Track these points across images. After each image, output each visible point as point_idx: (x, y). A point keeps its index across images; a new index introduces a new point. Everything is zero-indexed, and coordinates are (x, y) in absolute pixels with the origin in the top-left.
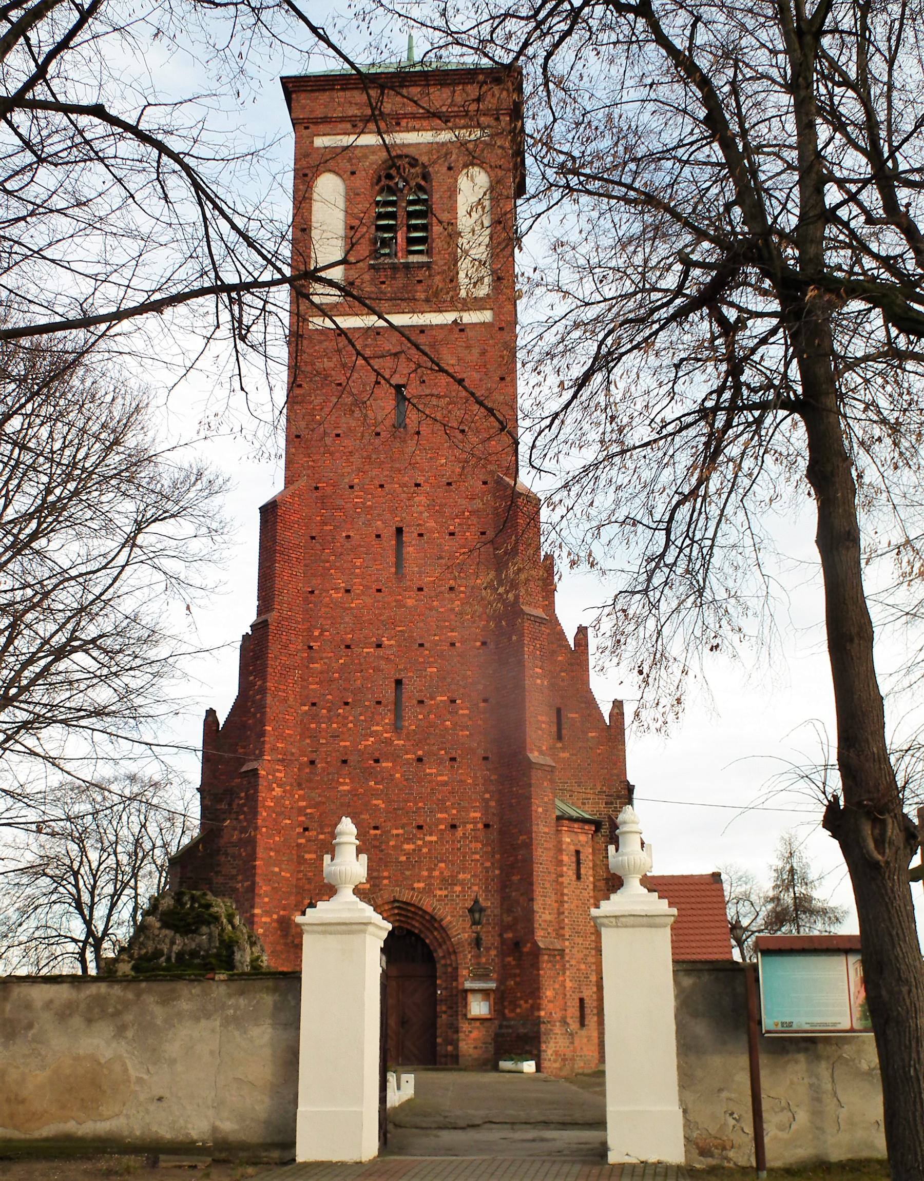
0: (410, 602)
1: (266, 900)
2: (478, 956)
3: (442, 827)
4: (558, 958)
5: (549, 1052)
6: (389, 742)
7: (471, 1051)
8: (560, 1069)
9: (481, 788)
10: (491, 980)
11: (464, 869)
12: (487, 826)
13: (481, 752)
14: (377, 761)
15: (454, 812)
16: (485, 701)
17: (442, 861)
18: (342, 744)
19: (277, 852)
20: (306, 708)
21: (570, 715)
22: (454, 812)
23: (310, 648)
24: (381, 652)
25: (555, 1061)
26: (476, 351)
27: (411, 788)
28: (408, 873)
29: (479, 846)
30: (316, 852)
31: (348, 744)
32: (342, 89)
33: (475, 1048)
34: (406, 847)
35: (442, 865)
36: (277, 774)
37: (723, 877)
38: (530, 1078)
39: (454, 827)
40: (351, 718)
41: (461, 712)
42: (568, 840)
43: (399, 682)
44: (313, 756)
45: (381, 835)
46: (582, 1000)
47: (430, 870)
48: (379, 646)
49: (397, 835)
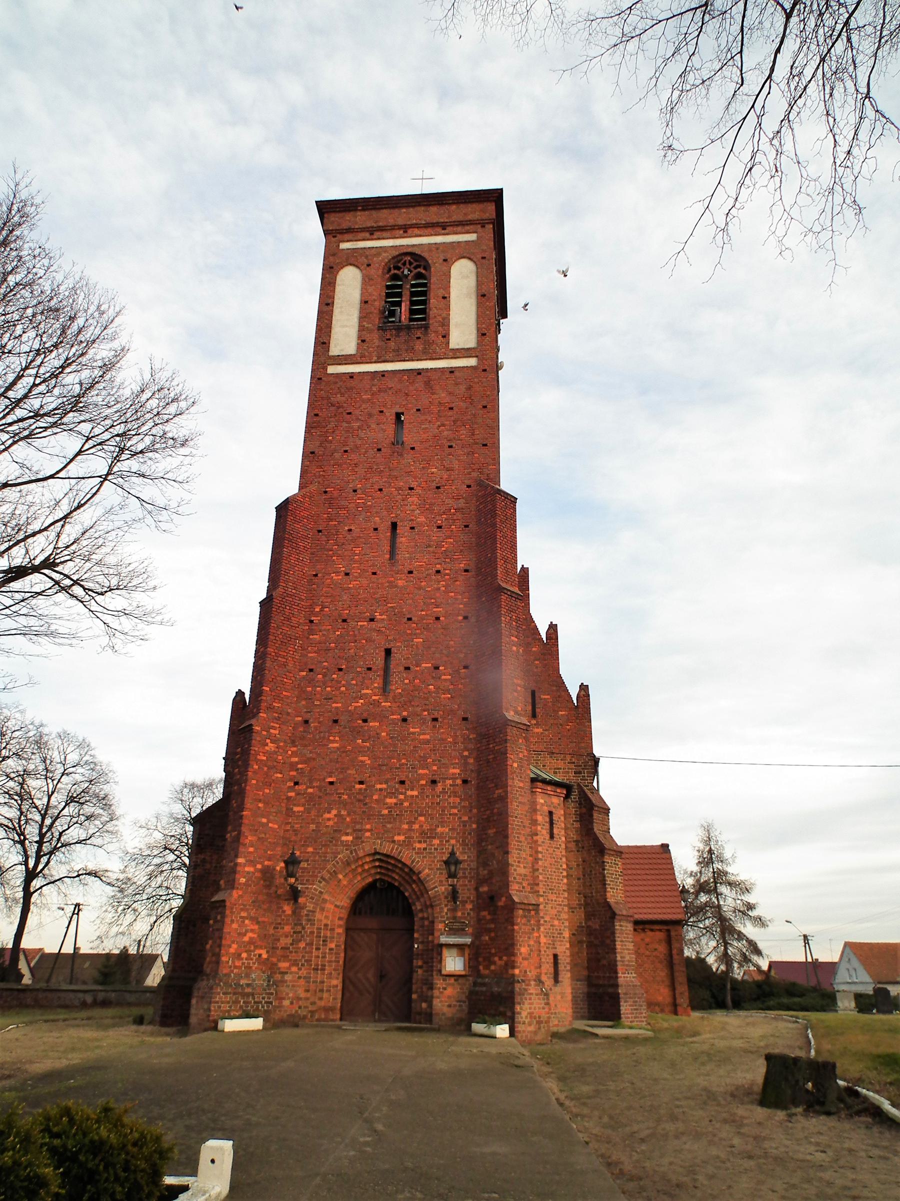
1: (251, 849)
2: (454, 910)
3: (423, 782)
5: (524, 1014)
6: (377, 704)
7: (445, 1009)
8: (535, 1033)
10: (467, 934)
11: (442, 823)
12: (465, 782)
14: (365, 721)
15: (435, 768)
18: (334, 705)
19: (266, 803)
20: (304, 673)
22: (435, 768)
24: (373, 625)
26: (463, 388)
27: (395, 745)
28: (389, 826)
30: (303, 805)
32: (363, 210)
33: (450, 1006)
34: (388, 800)
35: (422, 819)
36: (272, 731)
39: (434, 782)
42: (542, 801)
44: (307, 716)
45: (366, 790)
46: (555, 956)
47: (411, 823)
48: (372, 620)
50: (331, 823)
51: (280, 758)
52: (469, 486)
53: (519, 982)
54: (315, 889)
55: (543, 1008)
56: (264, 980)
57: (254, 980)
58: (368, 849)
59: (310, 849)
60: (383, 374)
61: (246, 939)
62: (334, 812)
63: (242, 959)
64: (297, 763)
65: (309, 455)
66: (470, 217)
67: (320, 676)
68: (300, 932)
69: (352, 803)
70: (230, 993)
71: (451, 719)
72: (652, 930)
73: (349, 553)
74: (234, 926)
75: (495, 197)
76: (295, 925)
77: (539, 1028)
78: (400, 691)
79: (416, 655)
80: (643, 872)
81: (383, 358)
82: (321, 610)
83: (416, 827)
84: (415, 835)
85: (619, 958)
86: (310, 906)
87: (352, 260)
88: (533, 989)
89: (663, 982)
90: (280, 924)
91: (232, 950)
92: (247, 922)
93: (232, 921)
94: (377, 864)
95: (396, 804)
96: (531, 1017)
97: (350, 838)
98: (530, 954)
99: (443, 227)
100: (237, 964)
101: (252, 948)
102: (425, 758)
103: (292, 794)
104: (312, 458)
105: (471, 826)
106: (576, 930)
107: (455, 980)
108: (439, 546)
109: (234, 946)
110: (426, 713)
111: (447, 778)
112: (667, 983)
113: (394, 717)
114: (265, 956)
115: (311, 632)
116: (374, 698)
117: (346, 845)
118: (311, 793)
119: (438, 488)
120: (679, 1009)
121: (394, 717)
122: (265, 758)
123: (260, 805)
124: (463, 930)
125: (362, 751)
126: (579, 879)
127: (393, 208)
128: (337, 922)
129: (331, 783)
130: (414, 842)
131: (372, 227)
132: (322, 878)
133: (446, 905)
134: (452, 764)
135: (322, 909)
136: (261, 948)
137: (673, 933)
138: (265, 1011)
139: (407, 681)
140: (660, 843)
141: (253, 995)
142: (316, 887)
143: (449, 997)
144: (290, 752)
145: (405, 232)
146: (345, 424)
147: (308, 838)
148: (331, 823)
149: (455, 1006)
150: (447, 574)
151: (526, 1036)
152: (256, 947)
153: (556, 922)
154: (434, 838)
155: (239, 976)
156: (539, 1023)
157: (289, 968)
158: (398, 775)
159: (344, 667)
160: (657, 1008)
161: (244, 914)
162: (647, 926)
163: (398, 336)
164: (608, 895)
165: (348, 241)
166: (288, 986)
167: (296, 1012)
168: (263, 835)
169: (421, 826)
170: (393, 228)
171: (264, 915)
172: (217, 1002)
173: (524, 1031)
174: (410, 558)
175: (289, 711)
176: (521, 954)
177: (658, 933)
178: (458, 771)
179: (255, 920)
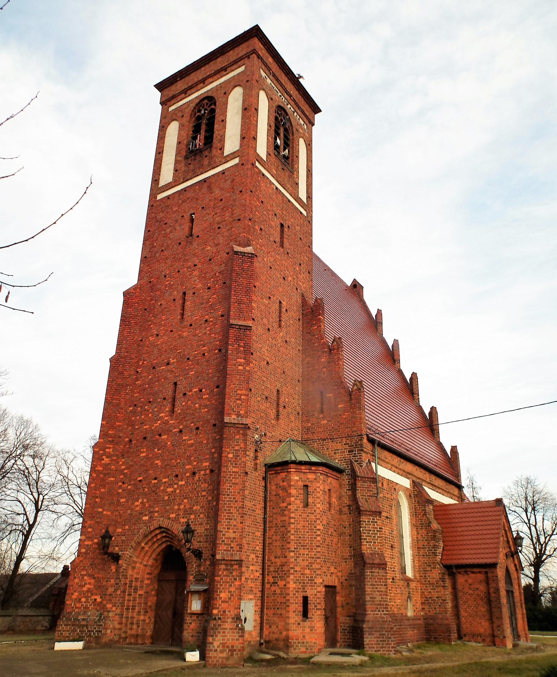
0: (185, 334)
1: (90, 530)
2: (199, 566)
3: (188, 474)
4: (235, 567)
5: (216, 644)
6: (167, 422)
7: (190, 638)
8: (227, 659)
9: (211, 445)
10: (205, 583)
11: (197, 503)
12: (212, 471)
13: (213, 422)
14: (160, 435)
15: (195, 463)
16: (217, 387)
17: (185, 499)
18: (145, 427)
19: (102, 498)
20: (131, 408)
21: (328, 395)
22: (195, 463)
23: (137, 372)
24: (169, 367)
25: (222, 652)
26: (229, 182)
27: (174, 450)
28: (168, 508)
29: (206, 485)
30: (125, 497)
31: (148, 426)
32: (181, 79)
33: (192, 636)
34: (169, 490)
35: (186, 501)
36: (107, 450)
37: (506, 502)
38: (193, 667)
39: (194, 474)
40: (151, 411)
41: (204, 397)
42: (297, 478)
43: (175, 384)
44: (131, 437)
45: (157, 483)
46: (305, 599)
47: (180, 504)
48: (168, 364)
49: (165, 482)
50: (138, 508)
51: (113, 467)
52: (228, 253)
53: (215, 619)
54: (128, 554)
55: (237, 640)
56: (96, 616)
57: (89, 616)
58: (155, 524)
59: (127, 527)
60: (185, 190)
61: (85, 589)
62: (140, 501)
63: (82, 602)
64: (124, 469)
65: (144, 259)
66: (240, 55)
67: (139, 409)
68: (118, 584)
69: (150, 494)
70: (70, 625)
71: (206, 427)
72: (473, 573)
73: (159, 321)
74: (76, 581)
75: (255, 33)
76: (117, 579)
77: (232, 655)
78: (180, 411)
79: (191, 383)
80: (475, 524)
81: (186, 179)
82: (143, 363)
83: (182, 507)
84: (181, 513)
85: (368, 598)
86: (124, 566)
87: (174, 117)
88: (228, 625)
89: (484, 616)
90: (109, 578)
91: (74, 597)
92: (85, 578)
93: (75, 578)
94: (164, 535)
95: (172, 492)
96: (223, 647)
97: (147, 518)
98: (230, 598)
99: (224, 70)
100: (77, 606)
101: (90, 594)
102: (189, 457)
103: (120, 491)
104: (146, 260)
105: (213, 503)
106: (348, 576)
107: (197, 617)
108: (208, 302)
109: (76, 594)
110: (193, 425)
111: (202, 470)
112: (487, 617)
113: (175, 430)
114: (99, 600)
115: (137, 379)
116: (166, 418)
117: (145, 523)
118: (130, 489)
119: (210, 260)
120: (497, 640)
121: (175, 430)
122: (101, 469)
123: (97, 500)
124: (203, 580)
125: (157, 457)
126: (350, 536)
127: (197, 70)
128: (146, 576)
129: (140, 481)
130: (181, 518)
131: (185, 89)
132: (131, 546)
133: (195, 563)
134: (205, 459)
135: (134, 568)
136: (96, 595)
137: (490, 575)
138: (96, 637)
139: (184, 404)
140: (494, 499)
141: (87, 626)
142: (128, 553)
143: (193, 630)
144: (121, 463)
145: (204, 83)
146: (163, 232)
147: (126, 519)
148: (138, 508)
149: (196, 636)
150: (211, 321)
151: (217, 661)
152: (92, 594)
153: (307, 571)
154: (192, 514)
155: (79, 613)
156: (232, 650)
157: (111, 608)
158: (175, 471)
159: (151, 400)
160: (479, 638)
161: (84, 573)
162: (468, 570)
163: (195, 160)
164: (364, 548)
165: (173, 104)
166: (110, 620)
167: (113, 638)
168: (99, 520)
169: (185, 506)
170: (197, 84)
171: (99, 573)
172: (60, 631)
173: (215, 657)
174: (191, 315)
175: (121, 435)
176: (220, 598)
177: (478, 575)
178: (207, 464)
179: (91, 576)
